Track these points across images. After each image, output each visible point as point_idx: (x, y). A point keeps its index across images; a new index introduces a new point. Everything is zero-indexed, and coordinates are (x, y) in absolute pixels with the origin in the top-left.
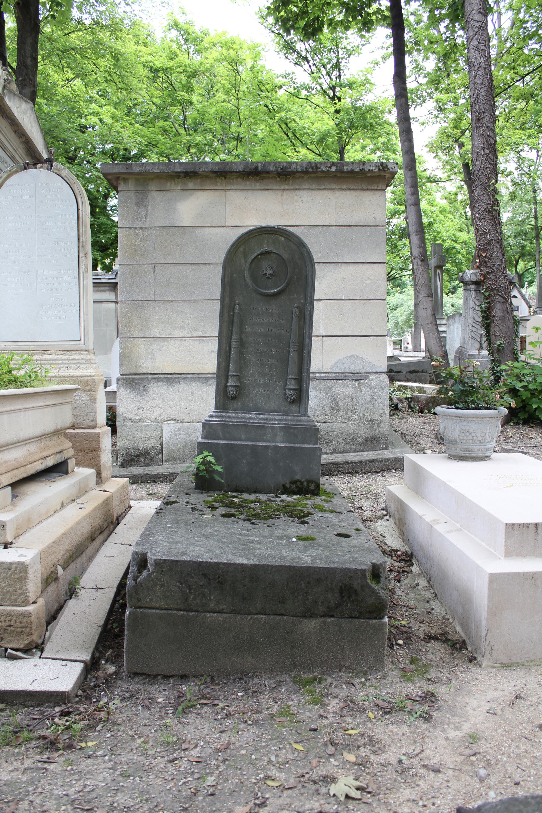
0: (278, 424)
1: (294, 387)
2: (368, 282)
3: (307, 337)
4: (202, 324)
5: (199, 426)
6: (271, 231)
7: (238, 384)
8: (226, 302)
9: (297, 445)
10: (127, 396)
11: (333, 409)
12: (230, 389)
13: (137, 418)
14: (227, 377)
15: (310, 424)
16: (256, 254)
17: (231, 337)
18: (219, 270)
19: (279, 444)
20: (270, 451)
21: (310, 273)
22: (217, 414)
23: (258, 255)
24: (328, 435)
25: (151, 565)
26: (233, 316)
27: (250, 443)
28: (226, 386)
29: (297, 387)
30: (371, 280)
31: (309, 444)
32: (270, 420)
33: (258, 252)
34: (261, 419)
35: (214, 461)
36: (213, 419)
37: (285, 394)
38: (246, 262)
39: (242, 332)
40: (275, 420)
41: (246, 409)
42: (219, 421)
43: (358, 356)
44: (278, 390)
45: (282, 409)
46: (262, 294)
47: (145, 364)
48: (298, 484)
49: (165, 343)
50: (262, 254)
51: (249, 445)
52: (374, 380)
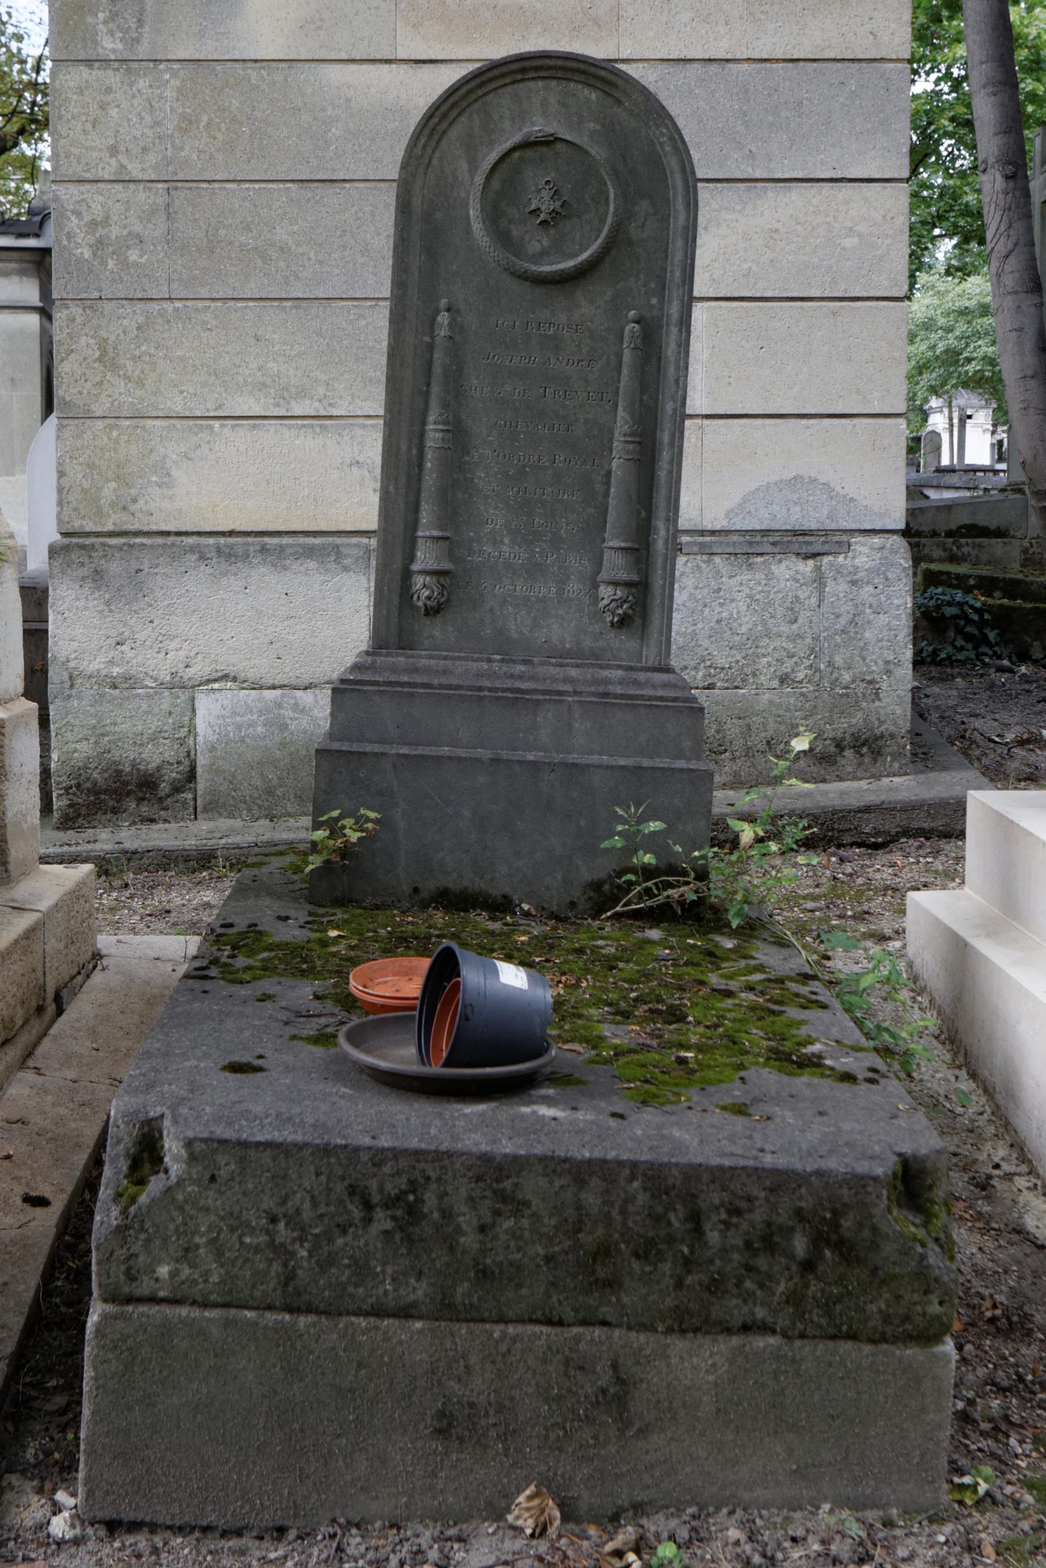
2: (850, 242)
4: (322, 377)
5: (325, 696)
7: (446, 565)
10: (81, 604)
12: (419, 581)
13: (116, 671)
16: (508, 145)
18: (388, 198)
25: (176, 1159)
28: (407, 575)
33: (517, 138)
36: (366, 677)
43: (813, 481)
46: (525, 277)
47: (141, 502)
49: (204, 436)
50: (526, 145)
52: (864, 554)
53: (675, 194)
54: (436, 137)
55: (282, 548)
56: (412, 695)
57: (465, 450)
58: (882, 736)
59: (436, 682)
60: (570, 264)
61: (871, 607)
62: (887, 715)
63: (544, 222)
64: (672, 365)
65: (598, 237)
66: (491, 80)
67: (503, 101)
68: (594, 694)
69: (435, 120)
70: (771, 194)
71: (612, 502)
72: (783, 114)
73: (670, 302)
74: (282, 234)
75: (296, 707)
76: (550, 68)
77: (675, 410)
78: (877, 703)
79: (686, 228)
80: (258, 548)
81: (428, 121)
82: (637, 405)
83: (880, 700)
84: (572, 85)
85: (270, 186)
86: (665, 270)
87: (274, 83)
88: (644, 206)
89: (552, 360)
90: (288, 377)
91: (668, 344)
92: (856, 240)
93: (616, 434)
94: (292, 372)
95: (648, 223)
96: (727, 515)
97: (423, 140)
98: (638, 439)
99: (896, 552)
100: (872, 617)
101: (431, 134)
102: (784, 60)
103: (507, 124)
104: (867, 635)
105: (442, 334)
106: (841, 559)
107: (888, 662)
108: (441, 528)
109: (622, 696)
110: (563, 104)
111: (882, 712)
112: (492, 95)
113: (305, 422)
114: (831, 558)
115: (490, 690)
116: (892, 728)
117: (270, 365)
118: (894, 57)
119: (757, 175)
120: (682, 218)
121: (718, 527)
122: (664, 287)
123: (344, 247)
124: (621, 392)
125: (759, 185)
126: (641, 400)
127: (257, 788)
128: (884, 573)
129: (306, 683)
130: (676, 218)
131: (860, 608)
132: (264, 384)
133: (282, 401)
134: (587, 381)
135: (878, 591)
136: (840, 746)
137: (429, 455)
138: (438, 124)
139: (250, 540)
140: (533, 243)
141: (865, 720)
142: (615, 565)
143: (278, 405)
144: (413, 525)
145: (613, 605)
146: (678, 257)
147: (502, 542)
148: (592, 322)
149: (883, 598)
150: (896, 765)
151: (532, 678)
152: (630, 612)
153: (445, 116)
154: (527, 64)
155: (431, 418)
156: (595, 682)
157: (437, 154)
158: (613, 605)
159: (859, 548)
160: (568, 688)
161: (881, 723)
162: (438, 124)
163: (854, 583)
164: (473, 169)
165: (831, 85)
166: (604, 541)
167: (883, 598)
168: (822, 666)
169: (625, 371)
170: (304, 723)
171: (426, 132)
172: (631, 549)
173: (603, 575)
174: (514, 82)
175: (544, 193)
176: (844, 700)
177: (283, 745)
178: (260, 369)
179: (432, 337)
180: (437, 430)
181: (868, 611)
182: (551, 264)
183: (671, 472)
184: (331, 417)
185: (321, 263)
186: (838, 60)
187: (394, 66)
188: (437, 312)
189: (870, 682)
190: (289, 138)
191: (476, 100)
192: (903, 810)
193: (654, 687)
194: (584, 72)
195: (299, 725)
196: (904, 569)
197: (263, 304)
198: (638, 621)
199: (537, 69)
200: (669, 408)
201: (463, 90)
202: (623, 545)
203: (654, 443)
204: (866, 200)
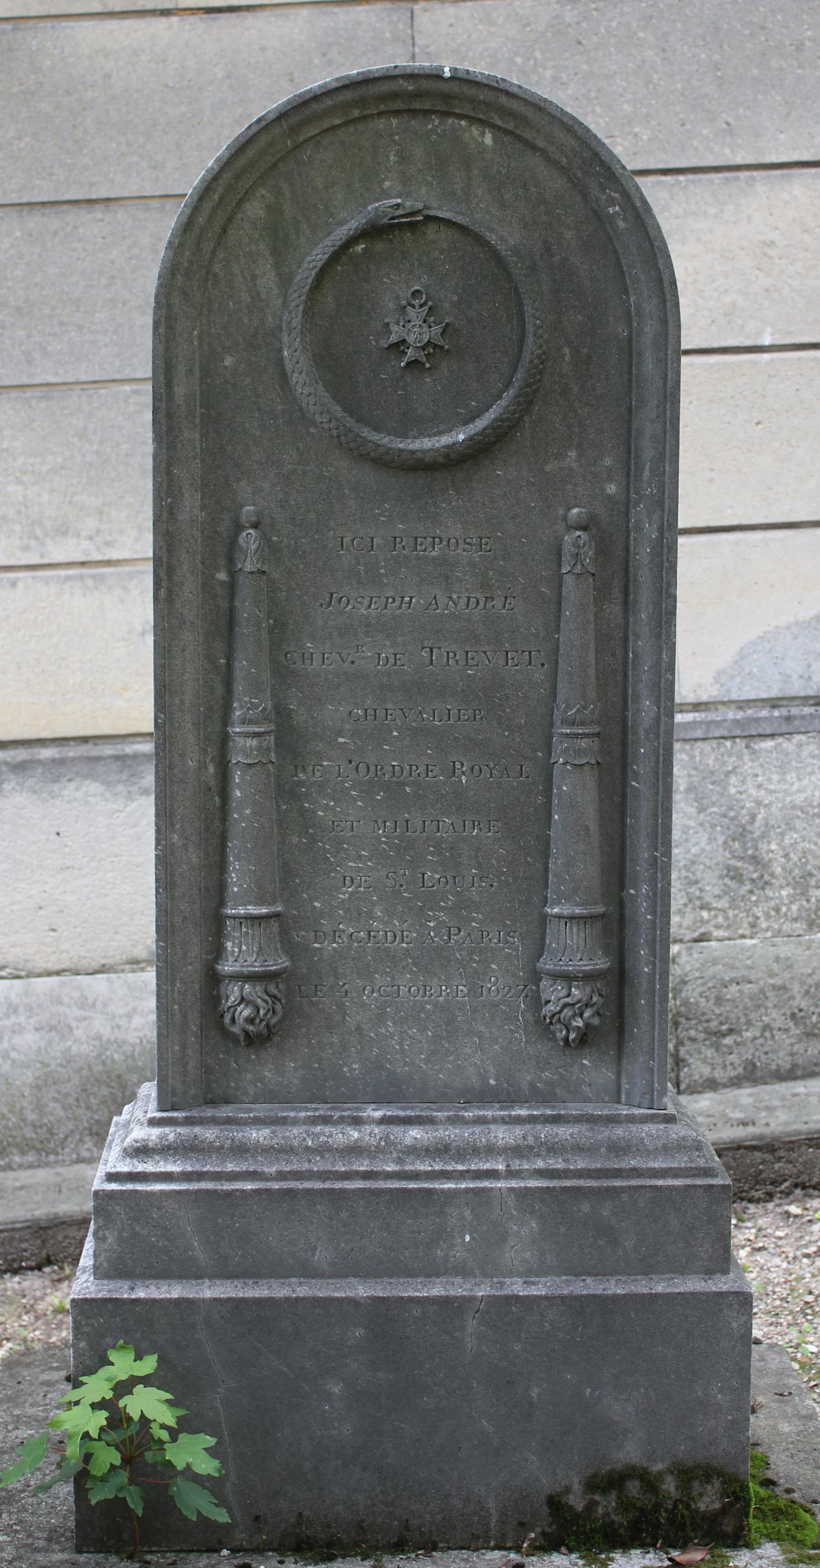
0: (511, 1174)
1: (587, 966)
3: (644, 689)
6: (418, 95)
7: (282, 962)
8: (183, 516)
9: (615, 1287)
11: (736, 876)
12: (233, 992)
14: (216, 926)
15: (680, 1161)
16: (342, 233)
17: (227, 709)
19: (517, 1287)
20: (471, 1324)
21: (650, 328)
22: (171, 1134)
23: (353, 240)
24: (719, 1001)
26: (232, 587)
27: (362, 1290)
28: (213, 980)
29: (601, 963)
31: (683, 1271)
32: (461, 1154)
33: (353, 225)
34: (414, 1151)
35: (168, 1417)
37: (537, 1003)
38: (285, 281)
39: (283, 674)
40: (491, 1150)
41: (331, 1093)
42: (186, 1177)
44: (498, 983)
45: (526, 1078)
48: (633, 1487)
50: (373, 231)
51: (353, 1302)
63: (413, 364)
70: (760, 188)
72: (774, 63)
75: (84, 1003)
89: (442, 599)
96: (717, 679)
113: (71, 572)
119: (739, 160)
121: (704, 698)
125: (743, 175)
129: (95, 965)
133: (33, 543)
143: (26, 548)
145: (568, 1013)
147: (370, 915)
152: (596, 1021)
158: (568, 1013)
166: (545, 902)
184: (109, 563)
187: (174, 20)
188: (239, 528)
190: (20, 138)
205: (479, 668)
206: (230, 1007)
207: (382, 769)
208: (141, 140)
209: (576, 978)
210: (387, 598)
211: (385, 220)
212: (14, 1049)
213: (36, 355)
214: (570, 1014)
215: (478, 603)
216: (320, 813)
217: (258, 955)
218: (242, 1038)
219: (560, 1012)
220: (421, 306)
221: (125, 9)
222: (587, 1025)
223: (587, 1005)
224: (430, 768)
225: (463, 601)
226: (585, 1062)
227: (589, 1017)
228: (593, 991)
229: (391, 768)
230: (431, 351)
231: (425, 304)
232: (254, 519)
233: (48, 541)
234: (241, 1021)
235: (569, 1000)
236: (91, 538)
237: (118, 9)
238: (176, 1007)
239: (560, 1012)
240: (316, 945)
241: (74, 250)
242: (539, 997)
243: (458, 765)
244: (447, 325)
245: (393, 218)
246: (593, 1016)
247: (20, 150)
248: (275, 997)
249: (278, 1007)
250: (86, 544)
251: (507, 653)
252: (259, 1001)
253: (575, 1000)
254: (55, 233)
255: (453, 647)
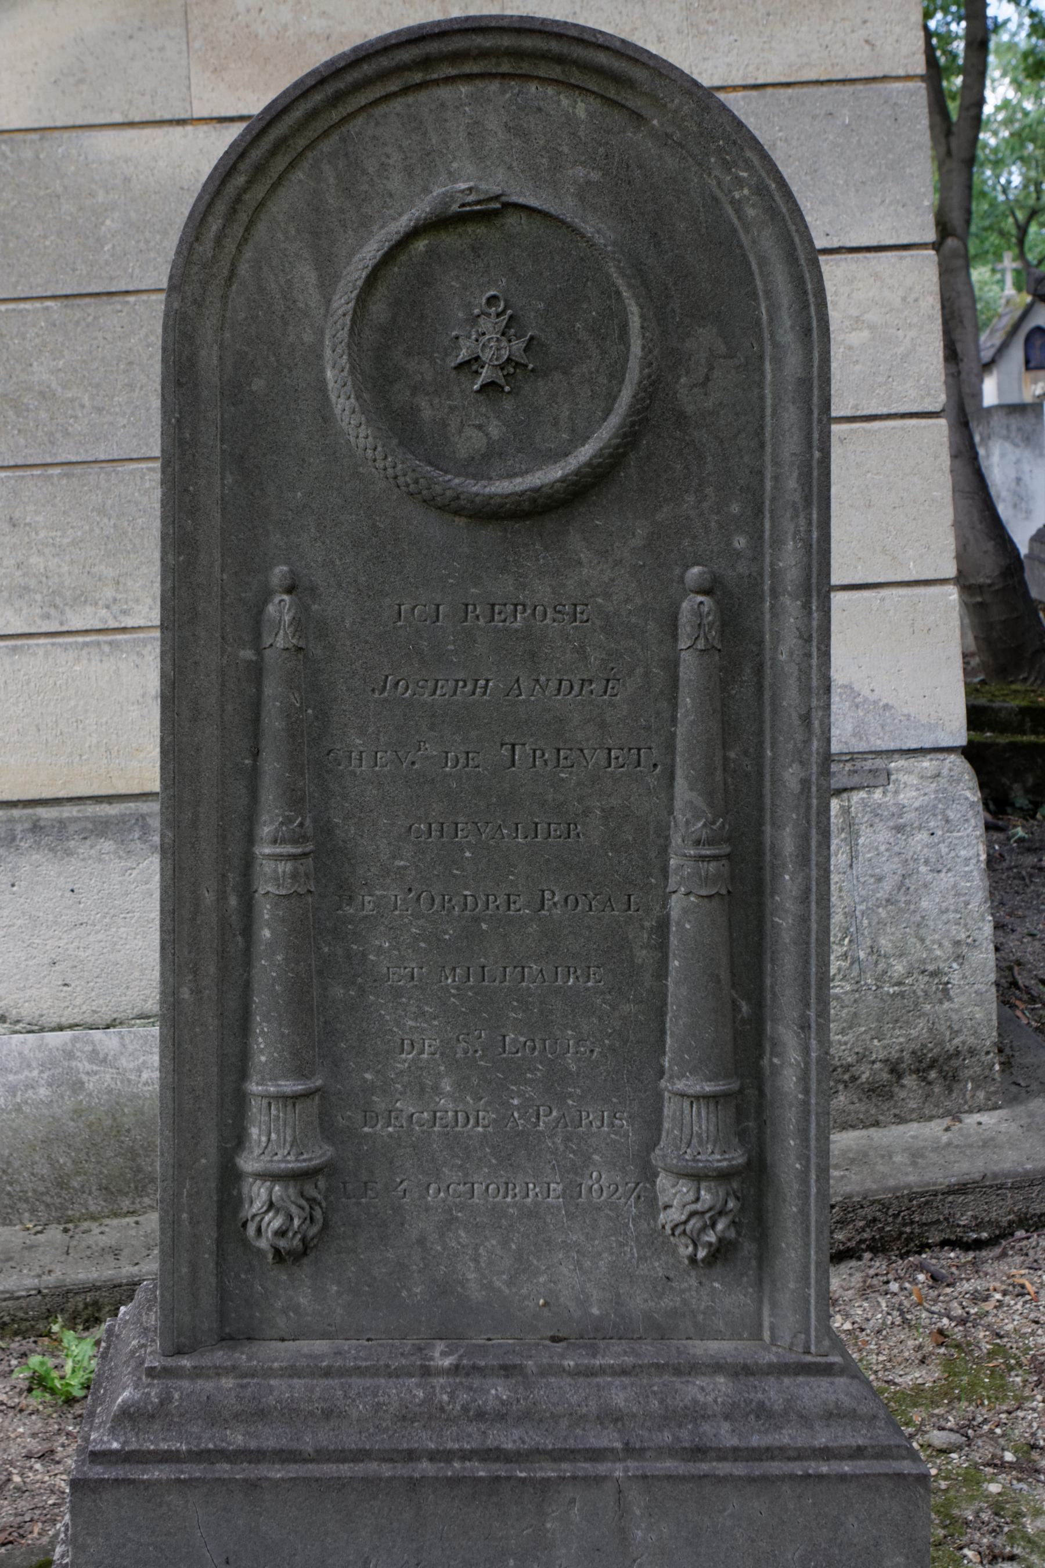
4: (109, 573)
7: (318, 1154)
16: (403, 223)
28: (230, 1177)
29: (738, 1157)
30: (872, 328)
33: (421, 209)
46: (453, 507)
52: (911, 786)
53: (773, 310)
54: (243, 217)
55: (62, 824)
56: (253, 1485)
57: (346, 892)
58: (957, 1053)
59: (308, 1443)
60: (552, 474)
61: (926, 862)
62: (963, 1021)
63: (490, 386)
64: (792, 682)
65: (608, 412)
66: (358, 87)
67: (384, 133)
68: (672, 1452)
69: (240, 180)
71: (676, 990)
73: (777, 543)
74: (41, 373)
75: (95, 1056)
76: (483, 54)
77: (805, 783)
78: (946, 1005)
79: (805, 382)
80: (27, 825)
81: (223, 182)
82: (719, 776)
83: (950, 999)
84: (533, 88)
85: (22, 306)
86: (760, 473)
87: (20, 162)
88: (704, 339)
90: (59, 575)
91: (777, 638)
92: (865, 334)
93: (676, 840)
94: (65, 569)
95: (717, 374)
97: (215, 225)
98: (726, 849)
99: (959, 781)
100: (929, 878)
101: (233, 211)
102: (745, 87)
103: (396, 182)
104: (924, 904)
105: (280, 643)
106: (878, 794)
107: (957, 943)
108: (301, 1073)
109: (736, 1454)
110: (516, 131)
111: (955, 1017)
112: (360, 120)
113: (88, 639)
114: (862, 794)
115: (433, 1456)
116: (971, 1041)
117: (33, 560)
118: (901, 72)
120: (793, 363)
122: (759, 512)
123: (131, 386)
124: (680, 746)
126: (726, 759)
127: (43, 1179)
128: (943, 813)
130: (778, 362)
131: (912, 865)
132: (26, 588)
133: (53, 611)
134: (602, 725)
135: (936, 839)
136: (896, 1070)
137: (265, 911)
138: (245, 189)
139: (16, 813)
140: (469, 432)
141: (930, 1030)
142: (690, 1127)
143: (47, 617)
144: (238, 1066)
145: (694, 1223)
146: (791, 446)
147: (436, 1089)
148: (607, 596)
149: (944, 850)
150: (981, 1095)
151: (527, 1417)
152: (732, 1234)
153: (259, 170)
154: (432, 47)
155: (266, 831)
156: (671, 1417)
157: (248, 254)
159: (903, 778)
160: (609, 1439)
161: (956, 1033)
162: (245, 189)
163: (899, 829)
164: (328, 282)
165: (814, 117)
167: (944, 850)
168: (862, 955)
169: (687, 701)
170: (108, 1077)
171: (221, 207)
172: (726, 1095)
173: (664, 1154)
174: (406, 90)
175: (485, 324)
176: (898, 1002)
177: (78, 1112)
178: (18, 566)
179: (259, 651)
180: (278, 857)
181: (923, 869)
182: (511, 476)
183: (804, 919)
185: (99, 410)
186: (822, 83)
187: (189, 128)
188: (266, 595)
189: (934, 974)
190: (45, 237)
191: (326, 134)
192: (1016, 1187)
193: (805, 1420)
194: (559, 59)
195: (98, 1081)
196: (972, 805)
197: (19, 473)
198: (748, 1247)
199: (454, 57)
200: (791, 776)
201: (298, 113)
202: (709, 1088)
203: (759, 852)
204: (876, 276)
205: (574, 769)
206: (254, 1216)
207: (450, 900)
208: (158, 237)
209: (706, 1177)
210: (457, 681)
211: (455, 207)
212: (26, 1103)
213: (59, 435)
214: (699, 1225)
215: (572, 688)
216: (372, 957)
217: (291, 1146)
218: (270, 1256)
219: (685, 1222)
220: (498, 315)
221: (144, 119)
222: (720, 1240)
223: (720, 1213)
224: (512, 898)
225: (553, 685)
226: (716, 1285)
227: (723, 1231)
228: (728, 1194)
229: (462, 899)
230: (512, 370)
231: (503, 312)
232: (288, 582)
233: (67, 608)
234: (270, 1234)
235: (698, 1207)
236: (107, 607)
237: (137, 119)
238: (185, 1216)
239: (685, 1222)
240: (366, 1129)
241: (95, 338)
242: (655, 1198)
243: (547, 895)
244: (532, 338)
245: (463, 205)
246: (728, 1227)
247: (45, 247)
248: (314, 1200)
249: (318, 1214)
250: (104, 612)
251: (610, 750)
252: (294, 1210)
253: (707, 1206)
254: (77, 323)
255: (541, 744)
